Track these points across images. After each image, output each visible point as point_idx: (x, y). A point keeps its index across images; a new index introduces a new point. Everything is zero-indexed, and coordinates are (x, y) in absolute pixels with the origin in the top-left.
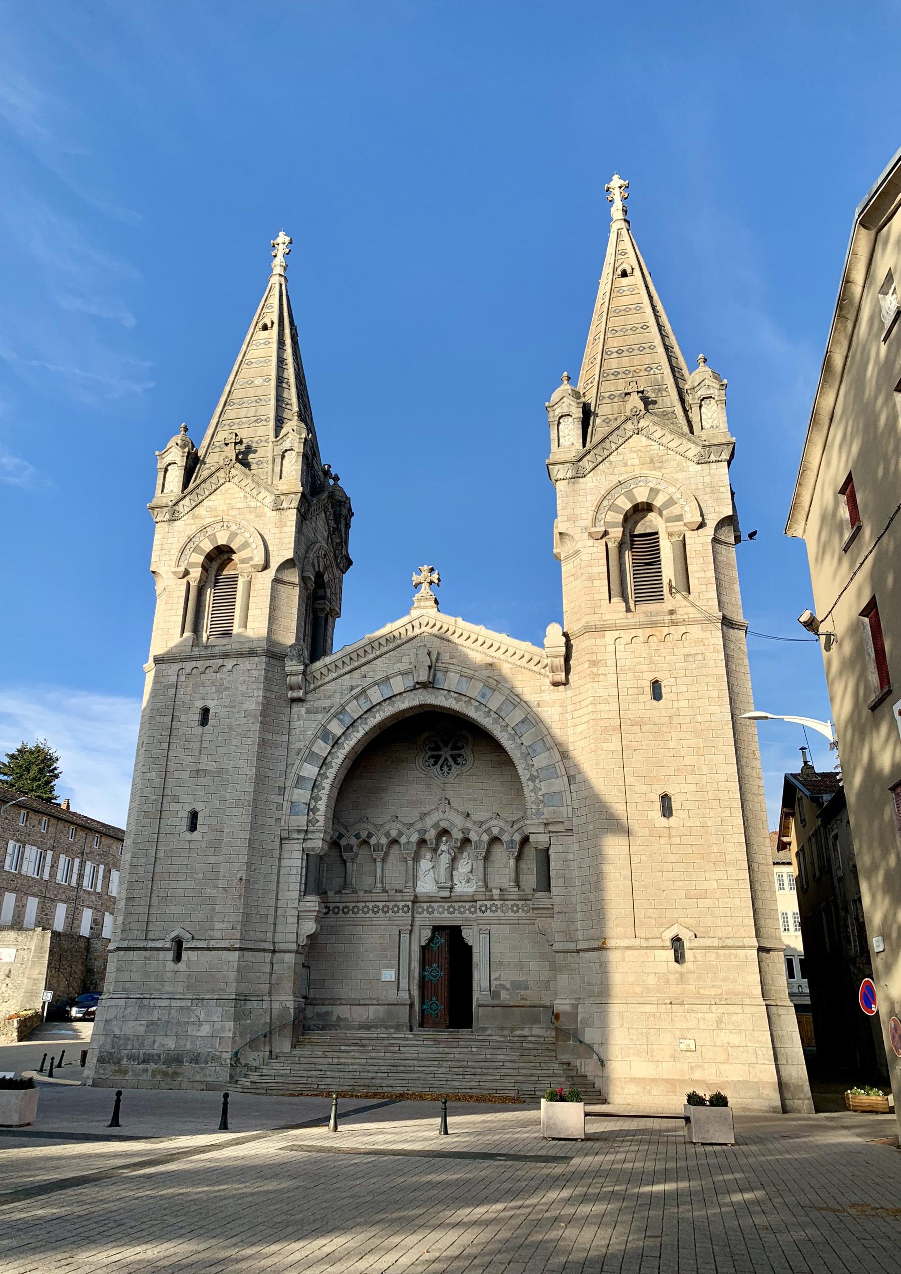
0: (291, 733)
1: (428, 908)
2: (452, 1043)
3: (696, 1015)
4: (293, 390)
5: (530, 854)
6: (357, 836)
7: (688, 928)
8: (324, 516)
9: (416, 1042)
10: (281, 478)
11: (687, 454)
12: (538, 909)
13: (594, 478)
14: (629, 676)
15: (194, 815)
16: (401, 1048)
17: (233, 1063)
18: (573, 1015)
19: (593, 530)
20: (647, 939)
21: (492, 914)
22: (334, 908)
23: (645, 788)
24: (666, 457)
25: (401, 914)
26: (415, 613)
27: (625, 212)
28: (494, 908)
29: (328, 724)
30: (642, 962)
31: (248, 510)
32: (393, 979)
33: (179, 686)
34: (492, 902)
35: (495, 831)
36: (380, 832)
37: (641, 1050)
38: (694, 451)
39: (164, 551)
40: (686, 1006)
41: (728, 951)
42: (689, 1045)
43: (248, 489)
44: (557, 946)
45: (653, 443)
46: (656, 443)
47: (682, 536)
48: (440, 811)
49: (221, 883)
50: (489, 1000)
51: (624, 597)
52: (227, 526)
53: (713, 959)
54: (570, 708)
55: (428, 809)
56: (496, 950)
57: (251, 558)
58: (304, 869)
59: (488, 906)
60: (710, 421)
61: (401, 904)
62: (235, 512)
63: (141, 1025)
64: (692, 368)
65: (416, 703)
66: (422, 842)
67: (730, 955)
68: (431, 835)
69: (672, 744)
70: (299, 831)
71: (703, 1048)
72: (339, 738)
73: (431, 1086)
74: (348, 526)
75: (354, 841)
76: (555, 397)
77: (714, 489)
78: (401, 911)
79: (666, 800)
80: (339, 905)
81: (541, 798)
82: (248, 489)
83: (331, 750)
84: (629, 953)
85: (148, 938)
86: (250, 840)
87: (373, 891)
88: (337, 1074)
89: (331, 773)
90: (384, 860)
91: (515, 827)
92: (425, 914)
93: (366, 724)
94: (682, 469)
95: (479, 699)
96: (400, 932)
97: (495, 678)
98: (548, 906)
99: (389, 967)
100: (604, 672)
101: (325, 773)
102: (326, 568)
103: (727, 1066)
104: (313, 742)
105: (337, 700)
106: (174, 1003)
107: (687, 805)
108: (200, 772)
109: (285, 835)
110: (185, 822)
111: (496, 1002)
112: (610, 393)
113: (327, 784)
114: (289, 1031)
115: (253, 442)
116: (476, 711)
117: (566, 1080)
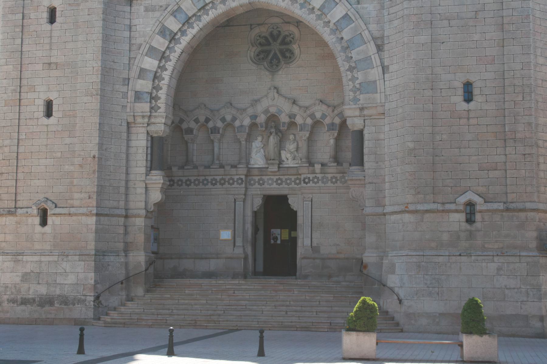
1: (259, 180)
6: (197, 121)
7: (479, 195)
16: (236, 292)
17: (96, 304)
20: (443, 204)
21: (314, 185)
22: (178, 181)
25: (235, 185)
29: (165, 21)
34: (314, 175)
37: (433, 292)
41: (511, 214)
49: (77, 161)
58: (149, 149)
61: (236, 178)
63: (17, 276)
66: (253, 125)
68: (262, 119)
69: (476, 37)
73: (259, 320)
75: (192, 125)
78: (235, 183)
84: (427, 215)
86: (100, 124)
96: (235, 200)
98: (361, 178)
99: (226, 228)
106: (43, 259)
108: (52, 65)
116: (301, 9)
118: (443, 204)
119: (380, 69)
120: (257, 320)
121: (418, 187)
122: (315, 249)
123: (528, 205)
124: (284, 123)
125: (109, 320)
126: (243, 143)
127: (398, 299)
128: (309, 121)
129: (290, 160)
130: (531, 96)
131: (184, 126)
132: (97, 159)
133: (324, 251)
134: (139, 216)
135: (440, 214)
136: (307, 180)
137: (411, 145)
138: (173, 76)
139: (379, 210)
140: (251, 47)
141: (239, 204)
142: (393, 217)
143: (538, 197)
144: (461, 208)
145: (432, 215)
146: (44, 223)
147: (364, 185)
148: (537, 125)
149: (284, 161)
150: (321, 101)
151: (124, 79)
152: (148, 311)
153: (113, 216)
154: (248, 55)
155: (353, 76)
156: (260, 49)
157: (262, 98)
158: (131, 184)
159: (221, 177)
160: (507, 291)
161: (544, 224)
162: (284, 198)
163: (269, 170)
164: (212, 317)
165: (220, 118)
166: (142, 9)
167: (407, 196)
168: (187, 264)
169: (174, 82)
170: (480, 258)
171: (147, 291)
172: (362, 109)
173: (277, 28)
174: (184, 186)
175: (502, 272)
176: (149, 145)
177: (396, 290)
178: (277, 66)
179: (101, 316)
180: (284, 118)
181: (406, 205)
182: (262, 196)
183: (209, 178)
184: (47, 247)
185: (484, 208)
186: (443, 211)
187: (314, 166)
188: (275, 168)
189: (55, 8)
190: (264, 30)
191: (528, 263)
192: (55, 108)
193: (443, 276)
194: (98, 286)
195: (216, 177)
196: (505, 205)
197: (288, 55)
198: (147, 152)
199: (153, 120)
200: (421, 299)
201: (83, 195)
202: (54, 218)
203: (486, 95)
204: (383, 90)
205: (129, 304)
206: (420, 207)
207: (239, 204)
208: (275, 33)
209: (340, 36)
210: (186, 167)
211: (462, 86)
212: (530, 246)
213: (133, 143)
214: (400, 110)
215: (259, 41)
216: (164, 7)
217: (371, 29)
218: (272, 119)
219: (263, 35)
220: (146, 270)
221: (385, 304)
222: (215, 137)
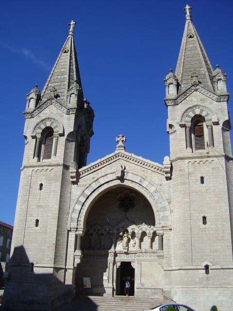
4: (74, 66)
5: (157, 238)
6: (105, 230)
11: (213, 98)
15: (37, 221)
18: (169, 292)
19: (181, 123)
20: (196, 266)
23: (197, 215)
26: (117, 152)
27: (190, 16)
38: (216, 97)
44: (165, 269)
49: (47, 245)
50: (140, 286)
51: (192, 148)
57: (58, 131)
62: (53, 115)
64: (214, 70)
70: (74, 228)
74: (93, 120)
76: (167, 77)
77: (221, 110)
79: (204, 218)
91: (140, 228)
94: (211, 103)
102: (84, 135)
109: (69, 229)
110: (34, 223)
118: (196, 266)
128: (140, 232)
137: (183, 242)
144: (203, 268)
160: (223, 303)
162: (130, 263)
191: (231, 291)
201: (48, 259)
222: (102, 237)
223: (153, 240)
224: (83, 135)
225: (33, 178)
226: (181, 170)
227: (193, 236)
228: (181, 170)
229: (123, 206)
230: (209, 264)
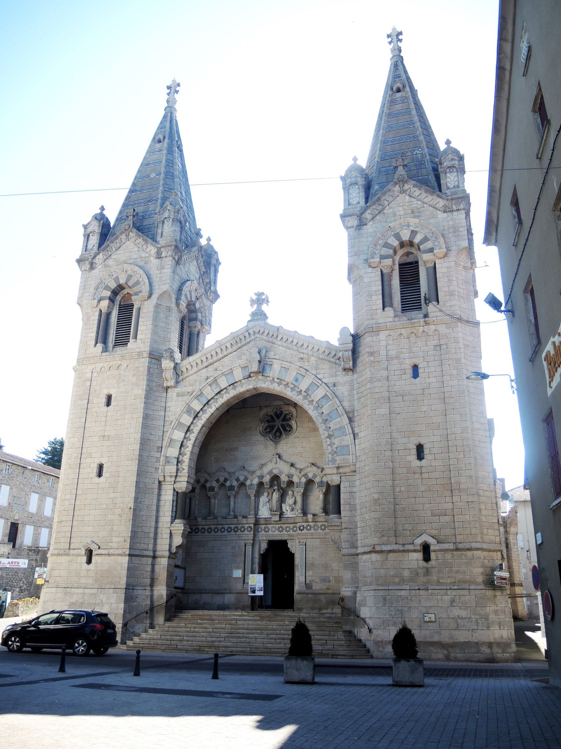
0: (166, 410)
1: (265, 528)
2: (273, 618)
3: (437, 597)
6: (218, 481)
7: (432, 537)
8: (196, 263)
9: (248, 618)
10: (161, 237)
12: (331, 526)
13: (373, 226)
14: (395, 362)
16: (238, 622)
17: (124, 630)
21: (307, 532)
22: (202, 529)
23: (405, 440)
24: (423, 209)
25: (246, 532)
28: (309, 528)
29: (191, 403)
30: (400, 561)
31: (140, 259)
32: (240, 576)
33: (92, 380)
34: (307, 524)
35: (310, 476)
36: (233, 478)
37: (397, 622)
39: (86, 290)
40: (430, 591)
41: (460, 553)
42: (430, 618)
43: (140, 246)
45: (413, 200)
46: (415, 200)
47: (433, 263)
48: (273, 462)
49: (118, 511)
52: (126, 271)
53: (449, 558)
54: (356, 386)
55: (266, 462)
56: (309, 556)
58: (175, 502)
59: (305, 526)
60: (453, 183)
61: (246, 526)
63: (66, 605)
65: (251, 387)
66: (261, 484)
67: (461, 555)
68: (267, 479)
69: (424, 409)
71: (441, 620)
72: (198, 413)
73: (252, 647)
74: (216, 271)
75: (214, 484)
78: (246, 530)
80: (205, 527)
81: (335, 450)
82: (140, 246)
83: (193, 421)
84: (391, 555)
85: (70, 548)
86: (136, 482)
87: (228, 517)
88: (191, 638)
89: (193, 436)
90: (235, 497)
92: (263, 532)
93: (217, 402)
95: (294, 382)
96: (245, 544)
97: (304, 367)
98: (338, 524)
99: (238, 568)
100: (378, 360)
101: (189, 437)
103: (456, 632)
104: (180, 416)
105: (197, 387)
106: (87, 591)
107: (434, 451)
108: (105, 437)
111: (308, 591)
112: (385, 168)
113: (190, 444)
114: (163, 612)
115: (146, 214)
116: (292, 391)
117: (345, 643)
118: (404, 545)
119: (352, 435)
120: (250, 647)
121: (382, 531)
122: (308, 586)
123: (474, 545)
124: (284, 482)
125: (131, 644)
126: (253, 498)
127: (368, 628)
128: (304, 480)
129: (289, 512)
130: (470, 454)
131: (208, 485)
132: (132, 510)
133: (317, 587)
134: (164, 557)
135: (402, 553)
136: (301, 528)
137: (376, 496)
138: (196, 445)
139: (353, 551)
140: (260, 423)
141: (249, 549)
142: (365, 557)
143: (482, 538)
144: (418, 548)
145: (394, 554)
146: (89, 561)
147: (341, 530)
148: (477, 477)
149: (284, 512)
150: (312, 464)
151: (158, 447)
152: (164, 637)
153: (143, 556)
154: (258, 429)
155: (331, 442)
156: (267, 424)
157: (267, 462)
158: (159, 530)
159: (235, 526)
160: (459, 621)
161: (489, 562)
163: (272, 519)
164: (214, 643)
165: (235, 478)
166: (175, 394)
167: (374, 538)
168: (206, 598)
169: (197, 450)
170: (435, 592)
171: (168, 619)
172: (338, 468)
173: (280, 408)
174: (206, 533)
175: (455, 604)
176: (175, 499)
177: (367, 620)
178: (280, 437)
179: (127, 641)
180: (284, 479)
181: (373, 546)
182: (267, 541)
183: (226, 527)
184: (90, 581)
185: (437, 547)
186: (404, 551)
187: (307, 516)
188: (277, 518)
189: (112, 395)
190: (270, 411)
192: (105, 470)
193: (405, 608)
194: (127, 615)
195: (231, 526)
196: (455, 545)
197: (288, 429)
198: (173, 504)
199: (178, 479)
200: (387, 628)
202: (97, 557)
203: (434, 454)
204: (354, 452)
205: (150, 631)
206: (385, 548)
207: (249, 549)
208: (278, 412)
209: (321, 412)
210: (208, 518)
211: (416, 448)
212: (478, 580)
213: (163, 498)
214: (367, 468)
215: (266, 419)
216: (191, 393)
217: (344, 405)
218: (275, 478)
219: (270, 414)
220: (167, 602)
221: (359, 633)
223: (305, 495)
224: (193, 299)
225: (94, 383)
226: (371, 354)
227: (396, 482)
228: (371, 354)
229: (269, 432)
230: (431, 541)
